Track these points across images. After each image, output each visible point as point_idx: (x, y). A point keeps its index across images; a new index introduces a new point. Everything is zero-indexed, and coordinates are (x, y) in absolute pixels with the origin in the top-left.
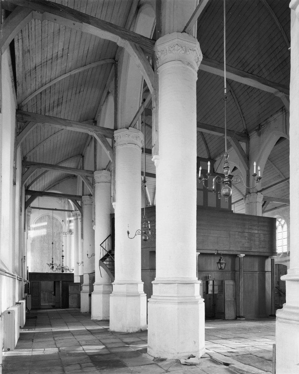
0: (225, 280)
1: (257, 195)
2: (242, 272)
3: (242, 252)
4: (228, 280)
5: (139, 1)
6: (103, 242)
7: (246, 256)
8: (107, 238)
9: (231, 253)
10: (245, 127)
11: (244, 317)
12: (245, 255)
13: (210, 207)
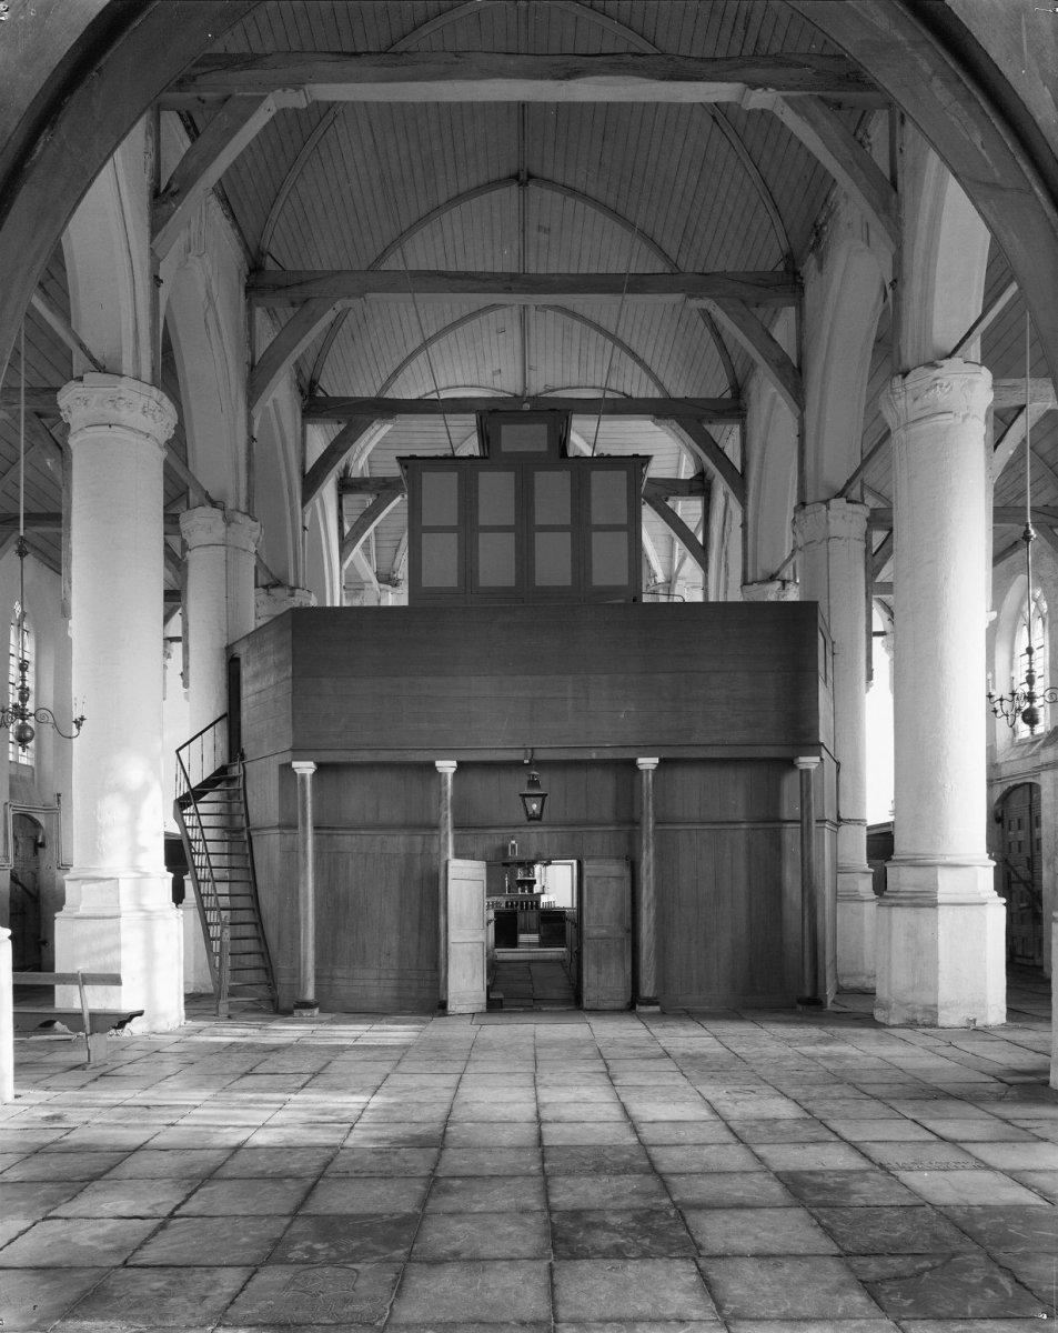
0: (588, 859)
1: (828, 508)
2: (814, 822)
3: (647, 750)
4: (602, 857)
5: (45, 11)
6: (203, 731)
7: (664, 763)
8: (211, 725)
9: (594, 756)
10: (784, 245)
11: (657, 1004)
12: (458, 763)
13: (542, 587)
